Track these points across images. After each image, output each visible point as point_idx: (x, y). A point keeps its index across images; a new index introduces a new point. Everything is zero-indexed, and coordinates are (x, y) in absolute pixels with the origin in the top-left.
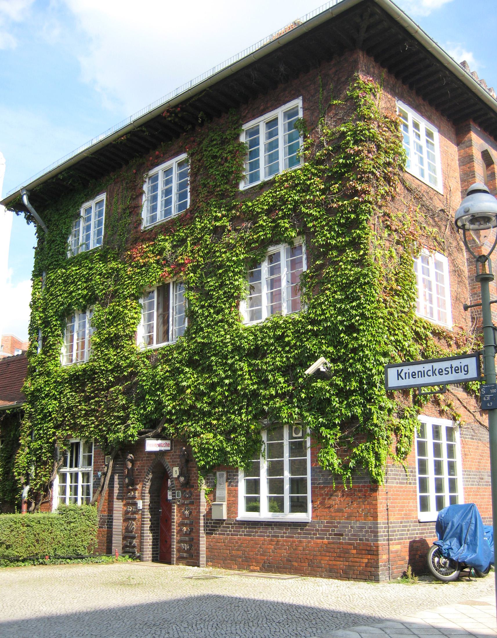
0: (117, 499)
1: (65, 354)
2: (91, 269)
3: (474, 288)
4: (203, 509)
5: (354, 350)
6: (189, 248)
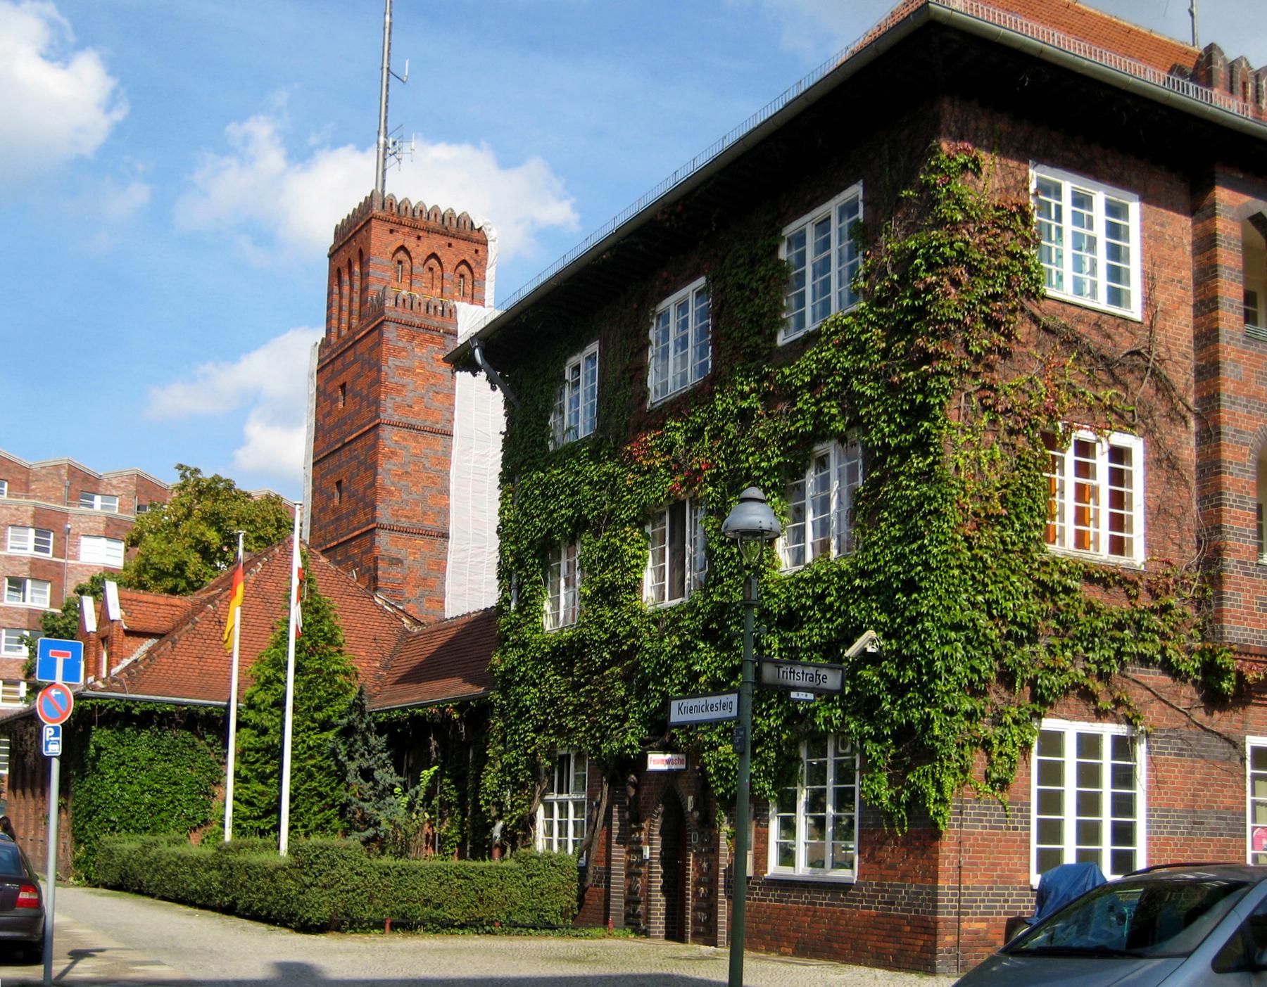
1: (549, 612)
2: (578, 473)
3: (1205, 487)
4: (724, 861)
5: (913, 621)
6: (707, 445)
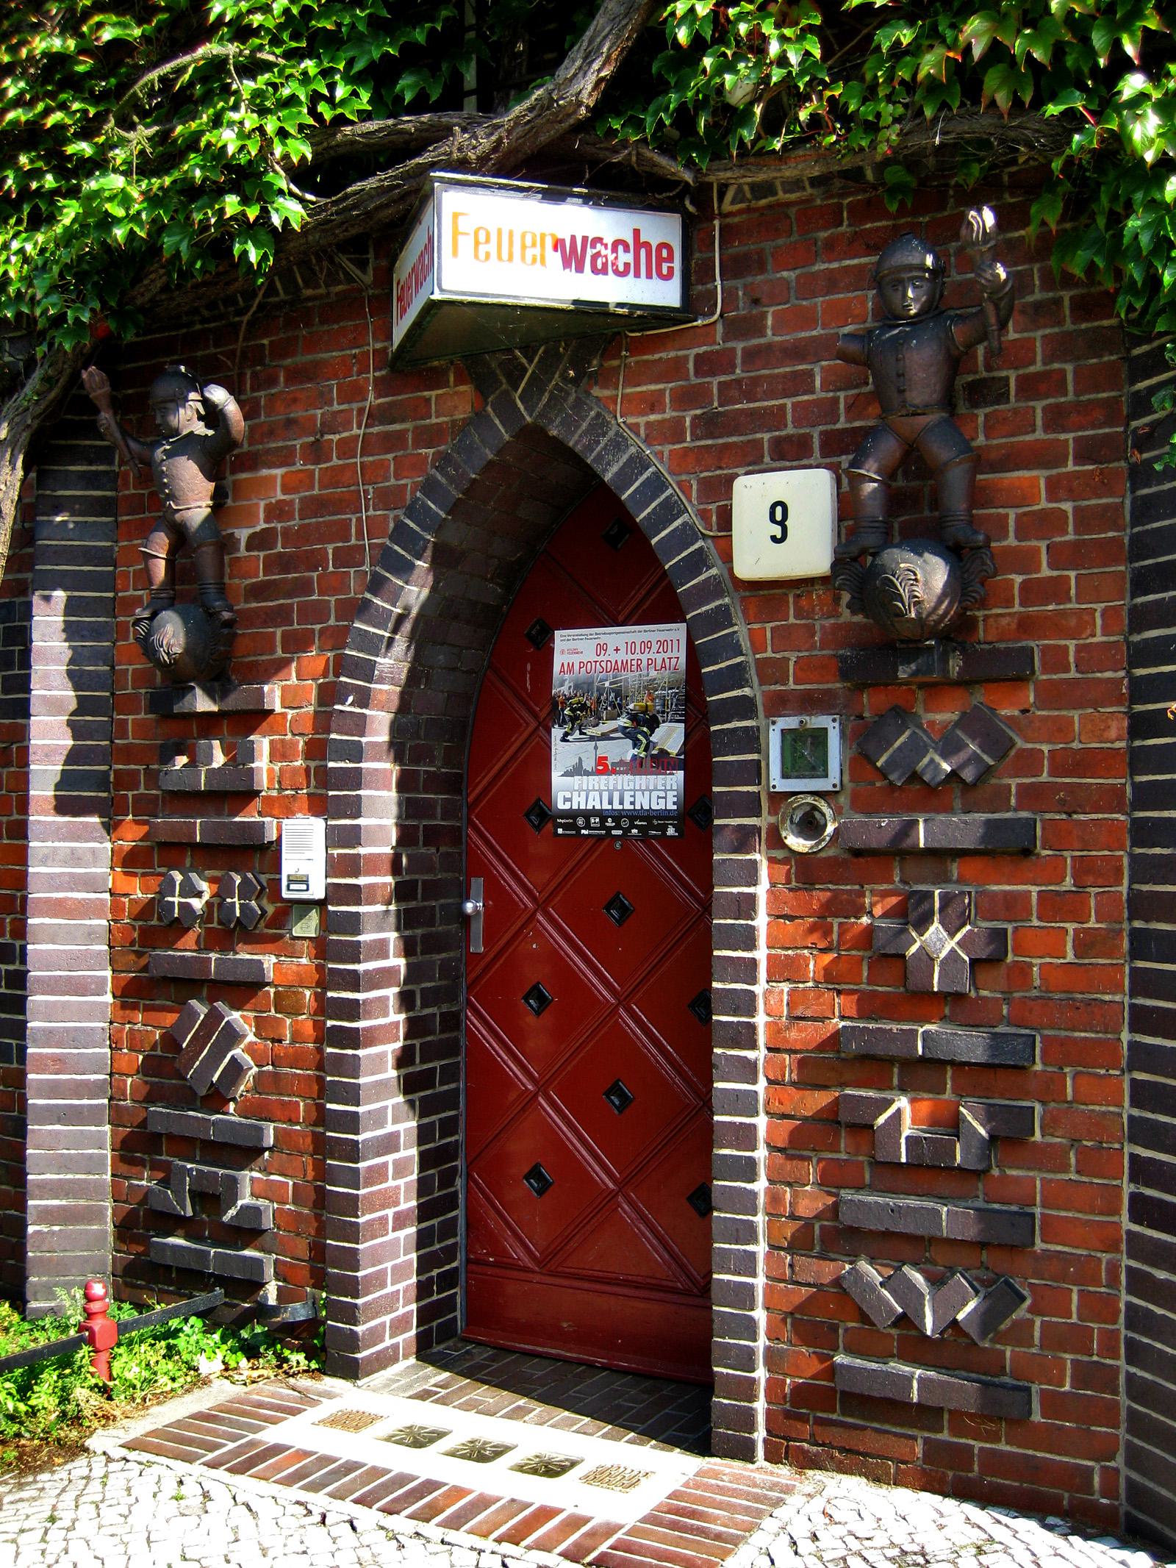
0: (63, 806)
